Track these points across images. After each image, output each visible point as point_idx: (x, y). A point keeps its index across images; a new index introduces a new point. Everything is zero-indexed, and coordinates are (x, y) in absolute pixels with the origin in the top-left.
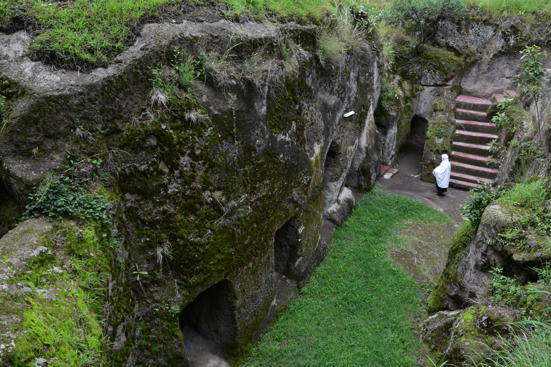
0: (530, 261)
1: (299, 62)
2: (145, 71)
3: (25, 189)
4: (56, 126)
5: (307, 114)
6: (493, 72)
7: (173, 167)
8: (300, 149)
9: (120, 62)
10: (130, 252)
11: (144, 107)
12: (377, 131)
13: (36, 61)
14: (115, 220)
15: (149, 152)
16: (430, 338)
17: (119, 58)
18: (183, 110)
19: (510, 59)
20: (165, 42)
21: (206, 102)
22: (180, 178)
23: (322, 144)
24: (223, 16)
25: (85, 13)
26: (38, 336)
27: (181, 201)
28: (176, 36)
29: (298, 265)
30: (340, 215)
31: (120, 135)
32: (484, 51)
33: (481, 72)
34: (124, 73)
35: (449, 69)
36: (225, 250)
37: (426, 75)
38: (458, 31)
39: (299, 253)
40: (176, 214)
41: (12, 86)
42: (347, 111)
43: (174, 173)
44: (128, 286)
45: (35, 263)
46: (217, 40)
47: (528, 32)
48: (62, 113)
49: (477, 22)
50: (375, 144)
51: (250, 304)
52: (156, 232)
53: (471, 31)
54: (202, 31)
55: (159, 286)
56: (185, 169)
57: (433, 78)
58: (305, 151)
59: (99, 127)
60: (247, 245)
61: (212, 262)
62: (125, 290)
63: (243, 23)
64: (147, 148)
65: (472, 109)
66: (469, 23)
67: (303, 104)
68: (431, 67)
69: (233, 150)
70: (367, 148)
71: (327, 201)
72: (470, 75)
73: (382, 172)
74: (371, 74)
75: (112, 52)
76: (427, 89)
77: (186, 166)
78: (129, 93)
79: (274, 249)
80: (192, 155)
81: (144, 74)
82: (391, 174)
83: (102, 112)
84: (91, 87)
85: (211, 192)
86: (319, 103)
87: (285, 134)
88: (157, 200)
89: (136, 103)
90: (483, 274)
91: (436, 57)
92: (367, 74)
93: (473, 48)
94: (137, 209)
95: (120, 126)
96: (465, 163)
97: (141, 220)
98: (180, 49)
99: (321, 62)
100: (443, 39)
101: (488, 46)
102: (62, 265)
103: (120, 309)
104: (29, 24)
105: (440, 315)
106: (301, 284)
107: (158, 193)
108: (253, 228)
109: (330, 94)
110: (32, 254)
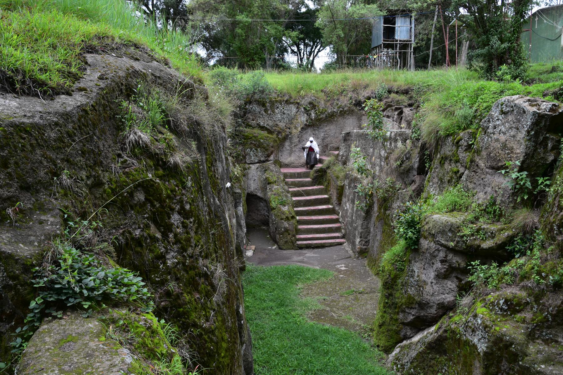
0: (503, 243)
3: (23, 273)
7: (166, 229)
16: (412, 370)
19: (314, 130)
22: (175, 243)
27: (183, 275)
31: (101, 190)
32: (292, 126)
33: (293, 145)
35: (268, 145)
38: (265, 112)
47: (323, 106)
49: (280, 102)
53: (276, 111)
57: (256, 156)
64: (136, 205)
65: (298, 178)
66: (274, 104)
76: (253, 167)
77: (178, 228)
80: (183, 213)
88: (157, 279)
90: (446, 281)
91: (254, 137)
93: (282, 125)
96: (311, 224)
100: (253, 121)
101: (295, 121)
105: (402, 348)
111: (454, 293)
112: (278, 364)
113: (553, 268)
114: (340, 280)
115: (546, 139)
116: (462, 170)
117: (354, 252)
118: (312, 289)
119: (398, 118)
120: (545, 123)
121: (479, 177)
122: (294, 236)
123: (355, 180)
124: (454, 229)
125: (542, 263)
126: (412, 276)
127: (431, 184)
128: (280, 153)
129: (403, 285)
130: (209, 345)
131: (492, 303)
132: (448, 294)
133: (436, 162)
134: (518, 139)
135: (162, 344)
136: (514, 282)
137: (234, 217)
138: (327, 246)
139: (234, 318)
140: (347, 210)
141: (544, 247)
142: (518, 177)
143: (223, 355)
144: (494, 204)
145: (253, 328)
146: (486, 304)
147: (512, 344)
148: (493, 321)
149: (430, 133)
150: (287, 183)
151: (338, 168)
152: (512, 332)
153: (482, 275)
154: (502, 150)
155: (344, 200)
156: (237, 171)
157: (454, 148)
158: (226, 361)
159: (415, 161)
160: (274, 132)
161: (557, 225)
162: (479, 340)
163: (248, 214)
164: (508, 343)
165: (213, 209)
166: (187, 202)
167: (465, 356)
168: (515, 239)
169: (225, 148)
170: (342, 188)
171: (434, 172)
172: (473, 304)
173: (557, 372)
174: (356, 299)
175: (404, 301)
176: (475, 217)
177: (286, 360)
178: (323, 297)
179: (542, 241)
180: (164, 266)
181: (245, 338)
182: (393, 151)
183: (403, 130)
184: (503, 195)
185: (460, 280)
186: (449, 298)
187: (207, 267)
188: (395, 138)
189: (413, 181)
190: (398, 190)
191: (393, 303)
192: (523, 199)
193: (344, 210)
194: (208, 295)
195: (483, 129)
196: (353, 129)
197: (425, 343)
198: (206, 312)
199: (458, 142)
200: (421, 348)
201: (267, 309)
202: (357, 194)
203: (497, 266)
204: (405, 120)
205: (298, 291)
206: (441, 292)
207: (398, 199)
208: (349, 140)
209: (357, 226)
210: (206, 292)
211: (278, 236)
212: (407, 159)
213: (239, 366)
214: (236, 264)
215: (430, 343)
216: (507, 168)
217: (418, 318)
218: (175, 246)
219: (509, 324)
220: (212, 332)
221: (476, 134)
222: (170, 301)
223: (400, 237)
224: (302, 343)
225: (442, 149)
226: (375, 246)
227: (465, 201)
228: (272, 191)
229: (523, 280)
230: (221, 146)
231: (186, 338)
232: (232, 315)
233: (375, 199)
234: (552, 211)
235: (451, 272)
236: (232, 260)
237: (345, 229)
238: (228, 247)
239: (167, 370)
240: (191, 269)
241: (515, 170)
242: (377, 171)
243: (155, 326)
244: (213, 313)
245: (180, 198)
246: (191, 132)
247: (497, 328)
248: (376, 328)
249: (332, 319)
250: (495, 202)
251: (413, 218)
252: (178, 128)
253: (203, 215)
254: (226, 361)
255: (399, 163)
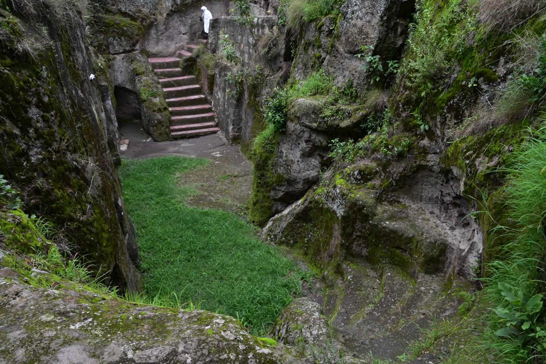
0: (358, 121)
6: (171, 30)
7: (25, 124)
16: (284, 238)
19: (181, 16)
22: (37, 139)
27: (51, 171)
32: (157, 12)
33: (160, 33)
35: (132, 34)
57: (121, 45)
65: (167, 68)
68: (115, 34)
76: (119, 57)
77: (38, 122)
80: (40, 105)
88: (22, 177)
91: (116, 24)
93: (145, 10)
96: (184, 115)
101: (159, 7)
105: (274, 221)
111: (317, 169)
112: (162, 248)
113: (398, 141)
114: (215, 166)
115: (396, 24)
116: (323, 55)
117: (227, 139)
118: (189, 177)
119: (265, 4)
120: (396, 9)
121: (339, 62)
122: (168, 127)
123: (225, 68)
124: (316, 111)
125: (389, 137)
126: (281, 157)
127: (296, 69)
128: (146, 42)
129: (273, 166)
130: (89, 236)
131: (349, 174)
132: (312, 170)
133: (301, 47)
134: (373, 24)
135: (35, 238)
136: (366, 155)
137: (102, 111)
138: (201, 136)
139: (113, 210)
140: (219, 98)
141: (391, 123)
142: (372, 61)
143: (104, 244)
144: (351, 86)
145: (134, 219)
146: (344, 176)
147: (364, 207)
148: (349, 190)
149: (295, 19)
150: (156, 74)
151: (208, 56)
152: (364, 197)
153: (340, 151)
154: (359, 35)
155: (216, 89)
156: (101, 62)
157: (317, 34)
158: (109, 250)
159: (282, 47)
160: (137, 19)
161: (402, 104)
162: (338, 207)
163: (118, 107)
164: (361, 207)
165: (76, 101)
166: (44, 94)
167: (327, 222)
168: (368, 117)
169: (84, 37)
170: (213, 77)
171: (299, 58)
172: (333, 176)
173: (398, 226)
174: (232, 182)
175: (274, 179)
176: (335, 100)
177: (170, 244)
178: (201, 184)
179: (390, 118)
180: (27, 163)
181: (128, 228)
182: (261, 38)
183: (269, 16)
184: (359, 78)
185: (322, 157)
186: (313, 173)
187: (76, 161)
188: (263, 24)
189: (280, 68)
190: (267, 77)
191: (265, 183)
192: (375, 81)
193: (216, 99)
194: (82, 189)
195: (343, 14)
196: (221, 16)
197: (293, 214)
198: (81, 206)
199: (320, 28)
200: (290, 219)
201: (147, 200)
202: (227, 82)
203: (353, 142)
204: (271, 6)
205: (176, 180)
206: (306, 169)
207: (267, 85)
208: (217, 27)
209: (229, 115)
210: (79, 186)
211: (151, 128)
212: (274, 45)
213: (124, 254)
214: (109, 157)
215: (297, 214)
216: (362, 52)
217: (287, 194)
218: (37, 142)
219: (362, 191)
220: (91, 224)
221: (337, 20)
222: (40, 199)
223: (269, 122)
224: (184, 226)
225: (306, 35)
226: (248, 132)
227: (326, 84)
228: (142, 83)
229: (374, 153)
230: (79, 33)
231: (63, 232)
232: (110, 207)
233: (245, 87)
234: (398, 91)
235: (315, 151)
236: (104, 154)
237: (218, 118)
238: (98, 141)
239: (45, 261)
240: (59, 164)
241: (370, 54)
242: (246, 59)
243: (25, 222)
244: (89, 206)
245: (36, 90)
246: (39, 16)
247: (353, 195)
248: (251, 207)
249: (210, 203)
250: (352, 84)
251: (280, 103)
252: (22, 10)
253: (66, 108)
254: (109, 250)
255: (266, 50)
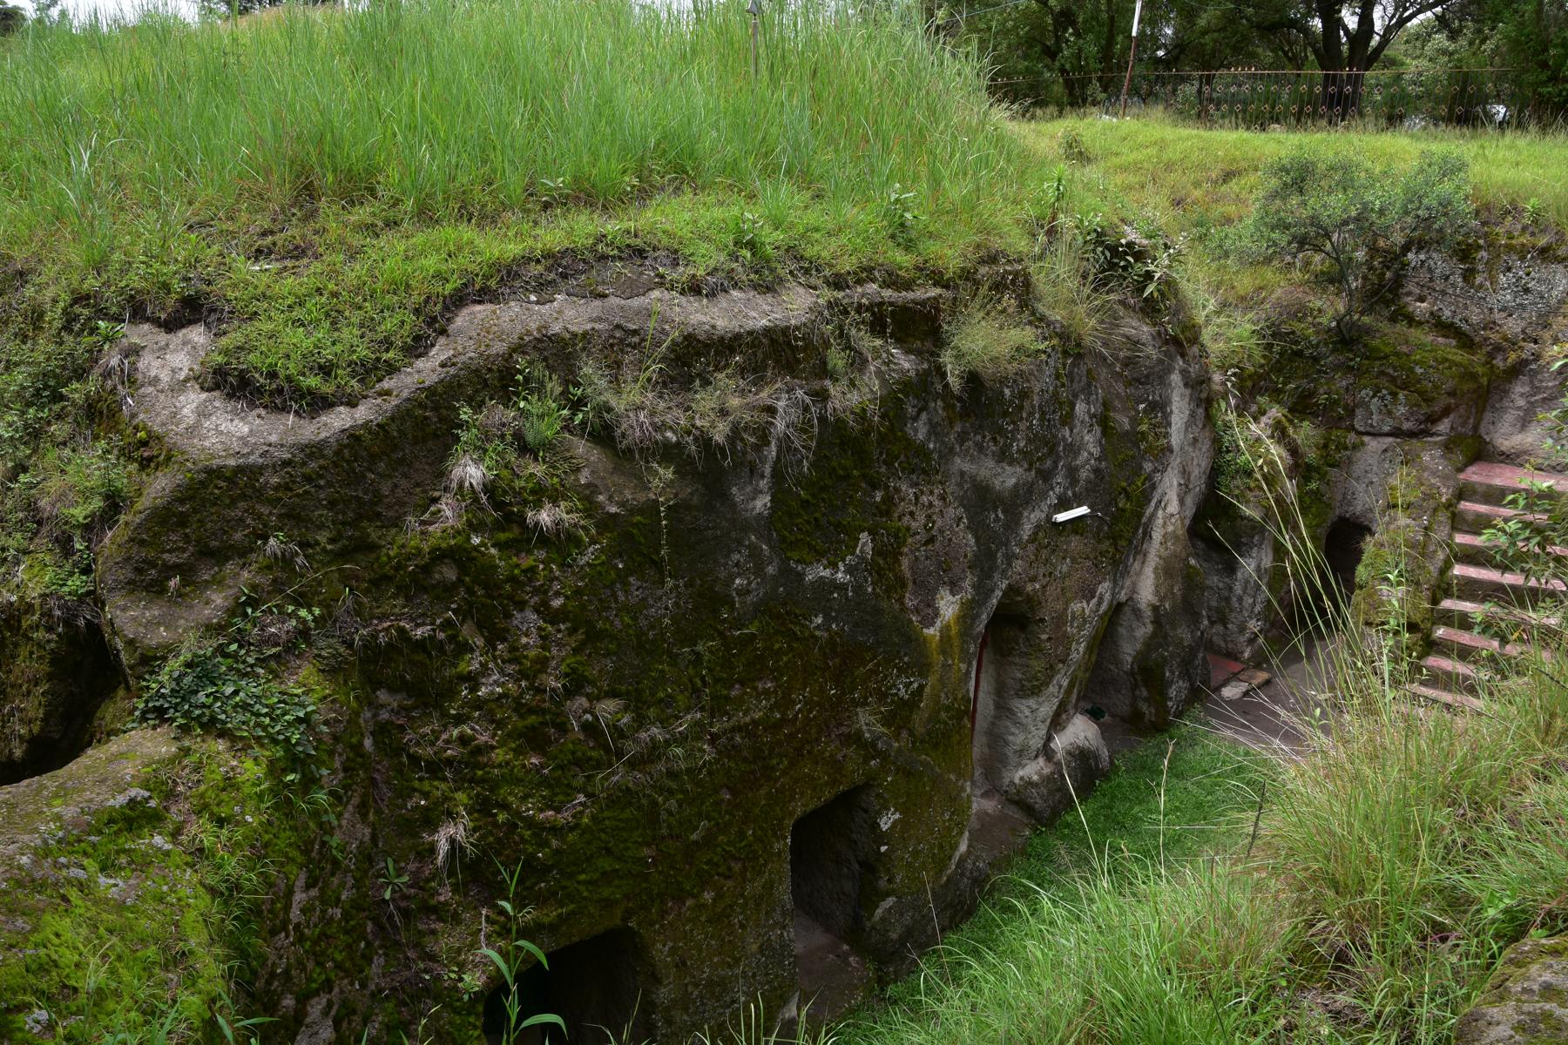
1: (884, 382)
2: (444, 412)
4: (225, 532)
5: (912, 514)
8: (884, 604)
9: (388, 393)
10: (374, 829)
11: (436, 494)
12: (1193, 562)
13: (209, 390)
14: (340, 748)
15: (437, 598)
17: (386, 384)
18: (525, 502)
20: (499, 348)
21: (588, 486)
22: (510, 661)
23: (968, 592)
24: (661, 281)
25: (331, 286)
26: (57, 966)
28: (529, 333)
29: (883, 919)
30: (1051, 792)
32: (1547, 335)
34: (392, 419)
36: (627, 849)
37: (1366, 406)
39: (883, 884)
40: (493, 748)
41: (152, 443)
42: (1064, 505)
43: (495, 649)
44: (361, 909)
45: (111, 821)
46: (636, 339)
48: (242, 504)
49: (1522, 253)
50: (1184, 597)
51: (703, 1004)
52: (443, 786)
54: (599, 319)
55: (440, 919)
56: (524, 640)
58: (903, 609)
59: (322, 537)
60: (696, 843)
61: (583, 877)
62: (346, 916)
63: (712, 295)
64: (434, 587)
67: (897, 490)
68: (1384, 381)
69: (665, 602)
70: (1155, 609)
71: (1009, 752)
72: (1506, 403)
73: (1217, 677)
74: (1159, 407)
75: (371, 371)
76: (1373, 445)
78: (401, 462)
79: (792, 863)
81: (440, 420)
82: (1244, 687)
83: (332, 504)
84: (313, 450)
85: (590, 701)
86: (959, 485)
87: (834, 566)
89: (418, 485)
91: (1397, 354)
92: (1142, 406)
93: (1513, 326)
94: (402, 728)
95: (374, 536)
97: (410, 756)
98: (531, 363)
99: (950, 379)
102: (175, 834)
103: (321, 959)
104: (212, 310)
106: (887, 973)
107: (452, 693)
108: (718, 803)
109: (998, 462)
110: (111, 802)
